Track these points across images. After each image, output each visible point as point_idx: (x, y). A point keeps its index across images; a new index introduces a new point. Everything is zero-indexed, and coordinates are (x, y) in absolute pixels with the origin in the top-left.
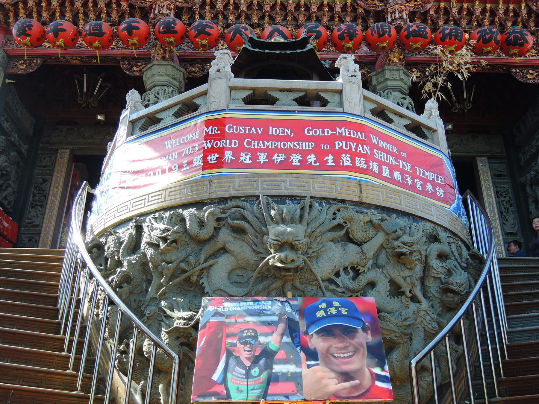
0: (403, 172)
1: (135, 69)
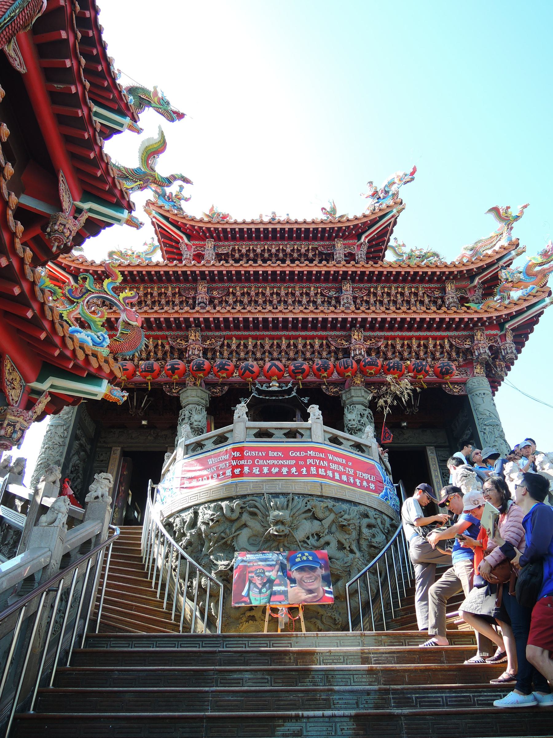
0: (348, 476)
1: (174, 391)
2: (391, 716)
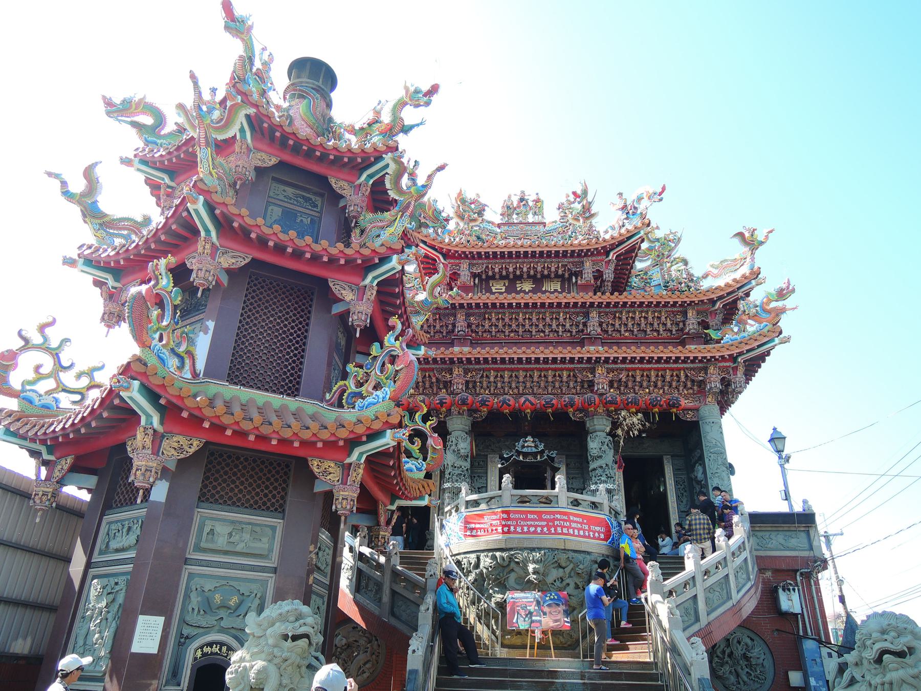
0: (584, 530)
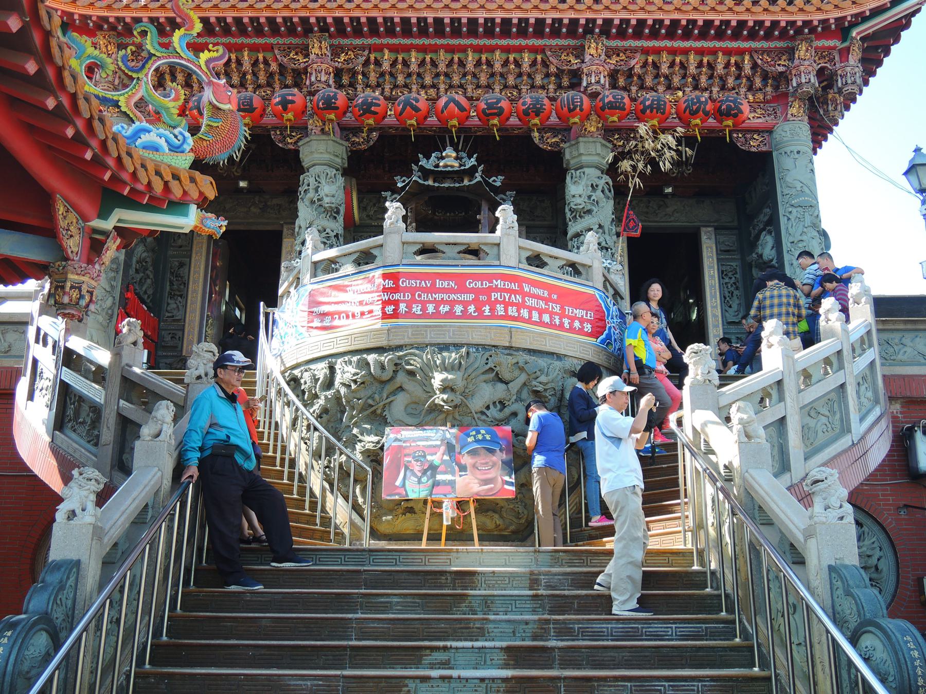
0: (552, 314)
1: (290, 141)
2: (544, 649)
